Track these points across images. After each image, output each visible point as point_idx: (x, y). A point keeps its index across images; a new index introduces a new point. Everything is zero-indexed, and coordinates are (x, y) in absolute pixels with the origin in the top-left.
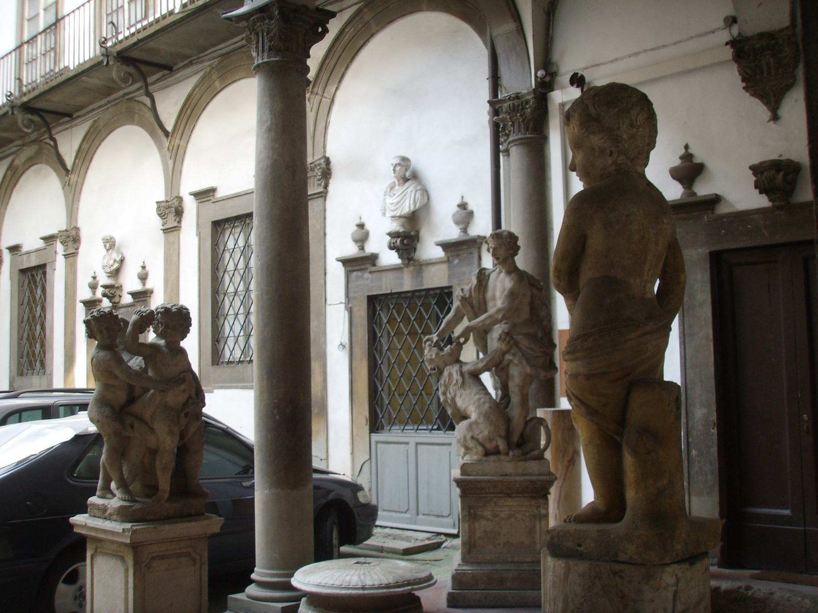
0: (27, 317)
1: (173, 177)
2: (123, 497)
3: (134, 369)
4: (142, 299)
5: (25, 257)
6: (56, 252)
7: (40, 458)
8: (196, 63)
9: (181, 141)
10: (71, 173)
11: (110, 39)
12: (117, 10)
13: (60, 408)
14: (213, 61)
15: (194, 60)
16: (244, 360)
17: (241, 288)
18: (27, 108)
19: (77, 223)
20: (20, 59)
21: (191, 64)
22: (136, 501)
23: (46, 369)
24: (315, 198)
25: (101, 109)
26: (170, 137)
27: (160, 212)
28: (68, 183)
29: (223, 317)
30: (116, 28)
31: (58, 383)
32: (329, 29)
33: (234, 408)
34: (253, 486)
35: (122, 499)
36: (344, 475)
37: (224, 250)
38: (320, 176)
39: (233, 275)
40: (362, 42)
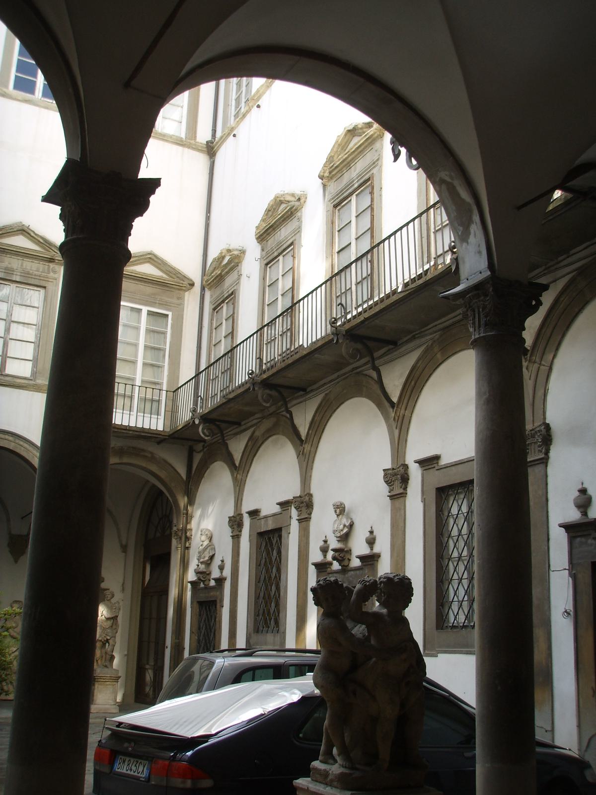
0: (263, 577)
1: (399, 446)
2: (344, 763)
3: (357, 637)
4: (370, 563)
5: (263, 521)
6: (291, 517)
7: (272, 716)
8: (418, 337)
9: (406, 411)
10: (305, 443)
11: (339, 318)
12: (345, 293)
13: (290, 667)
14: (435, 335)
15: (417, 334)
16: (468, 625)
17: (465, 553)
18: (266, 384)
19: (310, 490)
20: (261, 340)
21: (414, 338)
22: (357, 769)
23: (280, 627)
24: (534, 465)
25: (332, 383)
26: (395, 408)
27: (387, 480)
28: (302, 452)
29: (447, 581)
30: (345, 309)
31: (290, 643)
32: (543, 302)
33: (456, 674)
34: (474, 757)
35: (343, 766)
36: (570, 750)
37: (448, 516)
38: (540, 442)
39: (457, 540)
40: (577, 310)
